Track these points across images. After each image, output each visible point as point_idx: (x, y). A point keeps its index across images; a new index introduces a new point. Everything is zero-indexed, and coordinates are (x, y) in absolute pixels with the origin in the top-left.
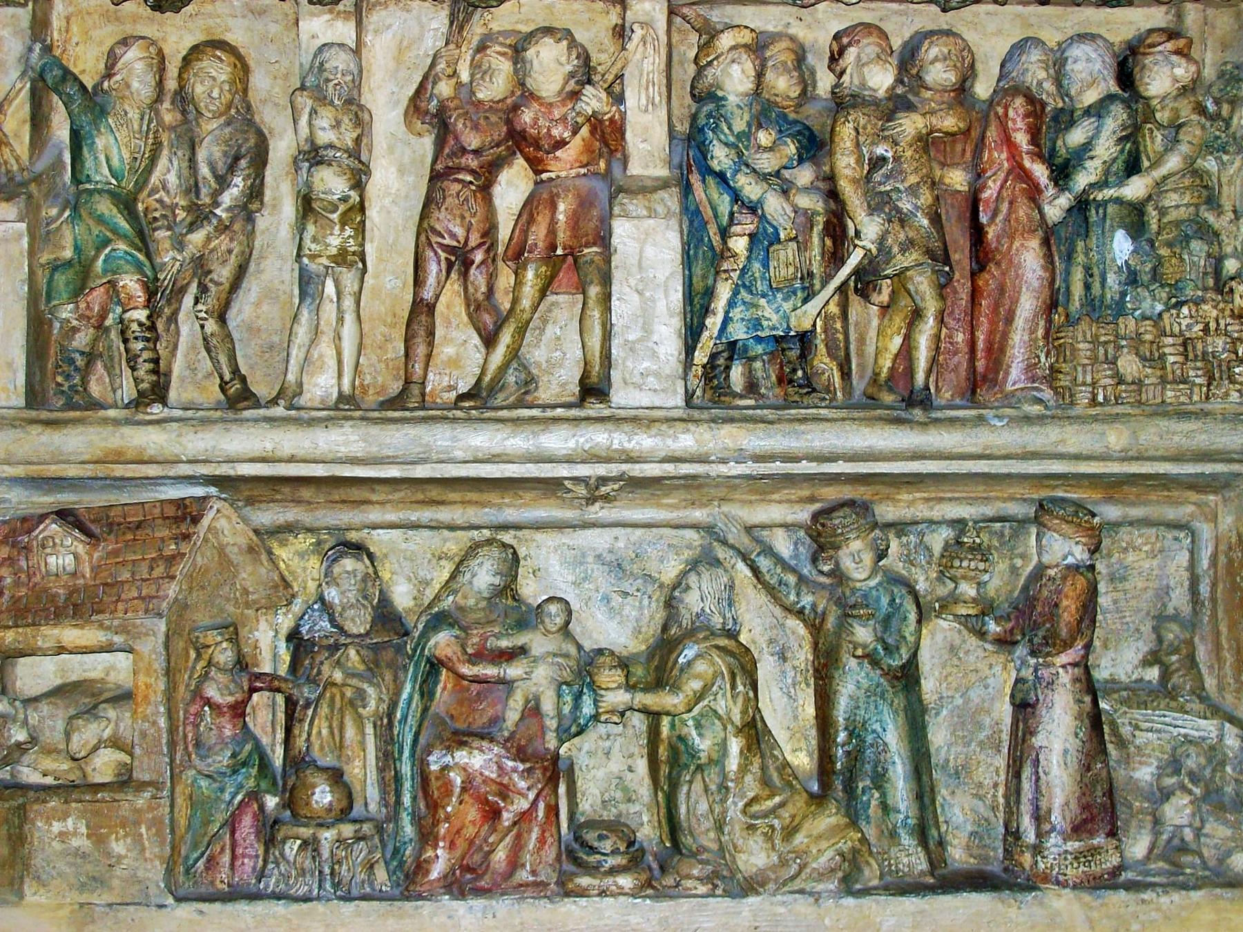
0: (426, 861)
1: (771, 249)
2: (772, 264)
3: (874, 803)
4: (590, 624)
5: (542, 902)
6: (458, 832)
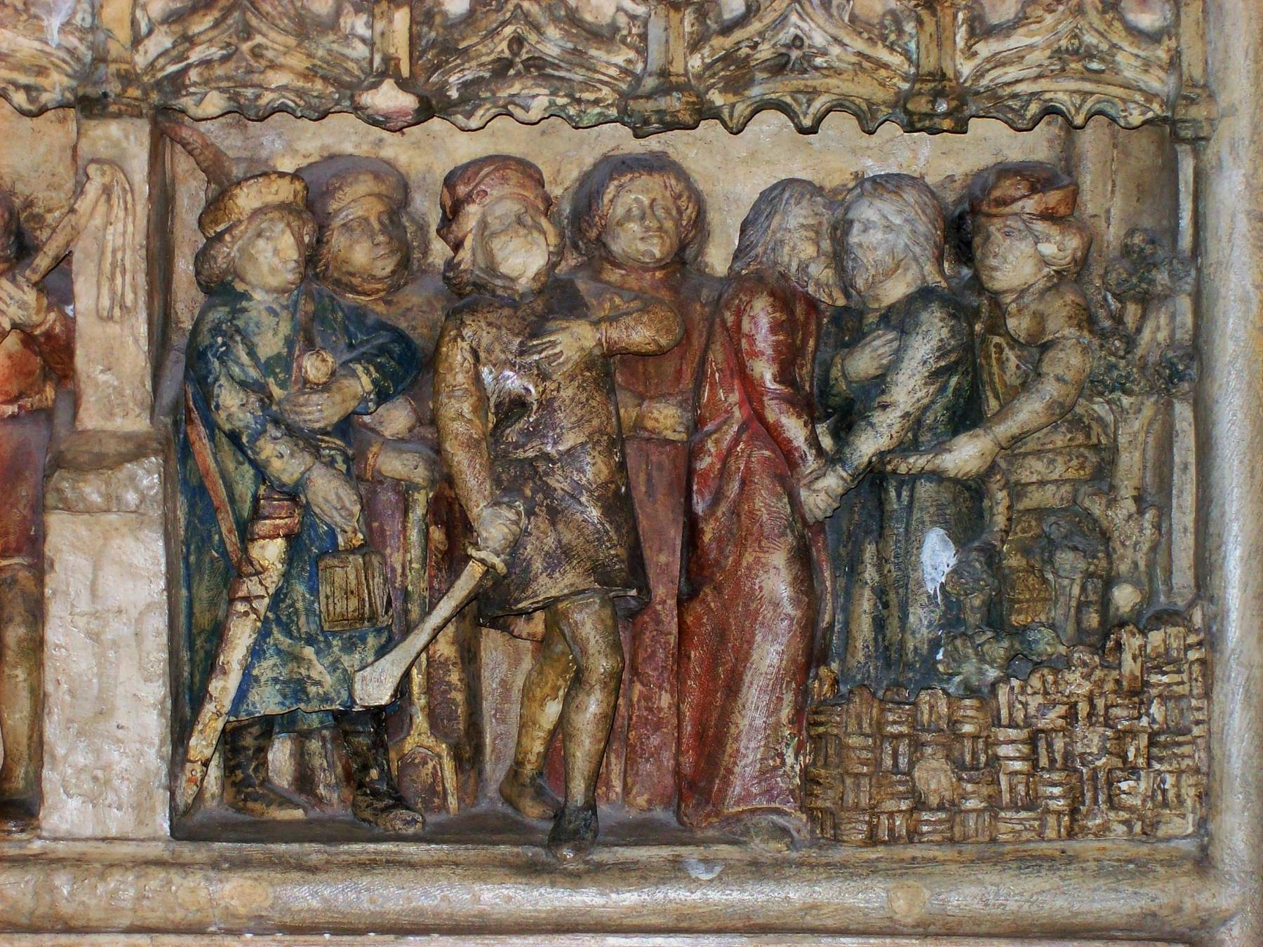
1: (322, 565)
2: (324, 589)
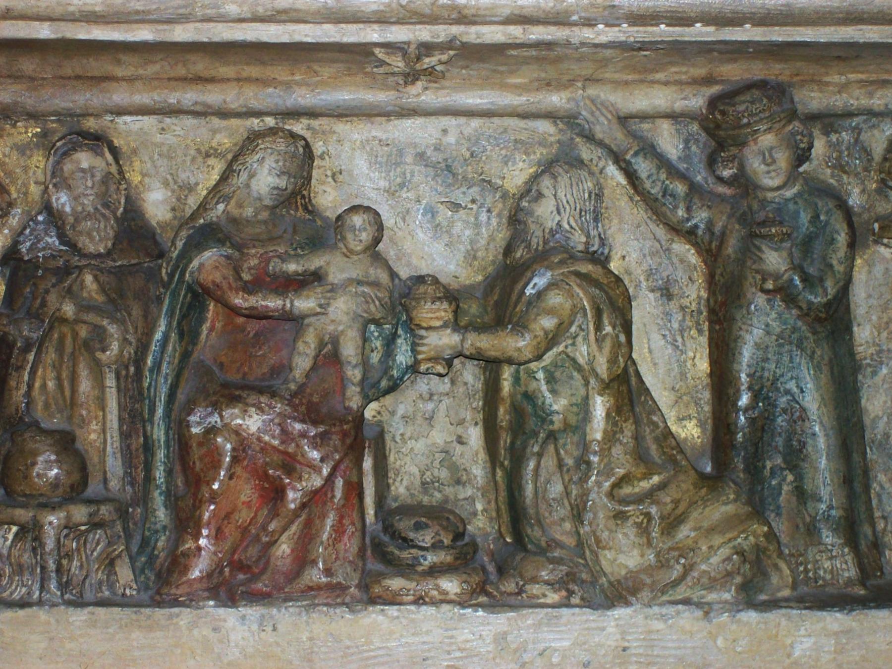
0: (186, 555)
3: (785, 488)
4: (408, 246)
5: (338, 611)
6: (228, 516)
